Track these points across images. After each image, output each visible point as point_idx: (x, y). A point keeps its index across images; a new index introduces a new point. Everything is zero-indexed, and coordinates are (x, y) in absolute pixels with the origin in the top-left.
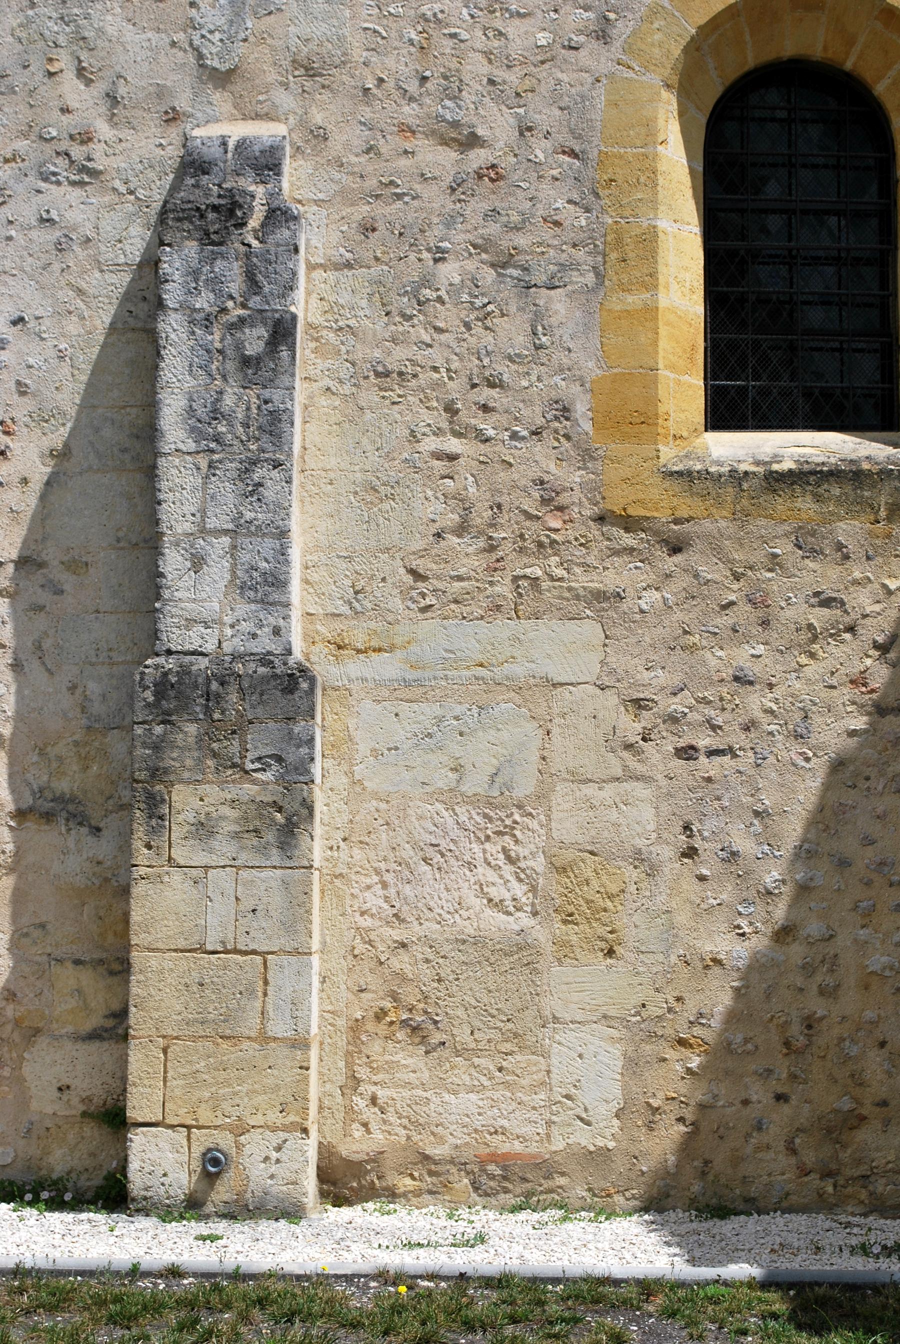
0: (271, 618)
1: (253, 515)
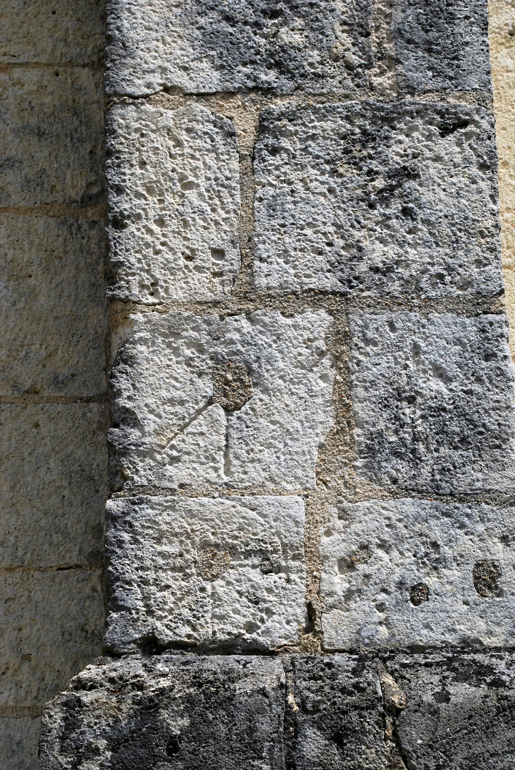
0: (465, 541)
1: (392, 251)
